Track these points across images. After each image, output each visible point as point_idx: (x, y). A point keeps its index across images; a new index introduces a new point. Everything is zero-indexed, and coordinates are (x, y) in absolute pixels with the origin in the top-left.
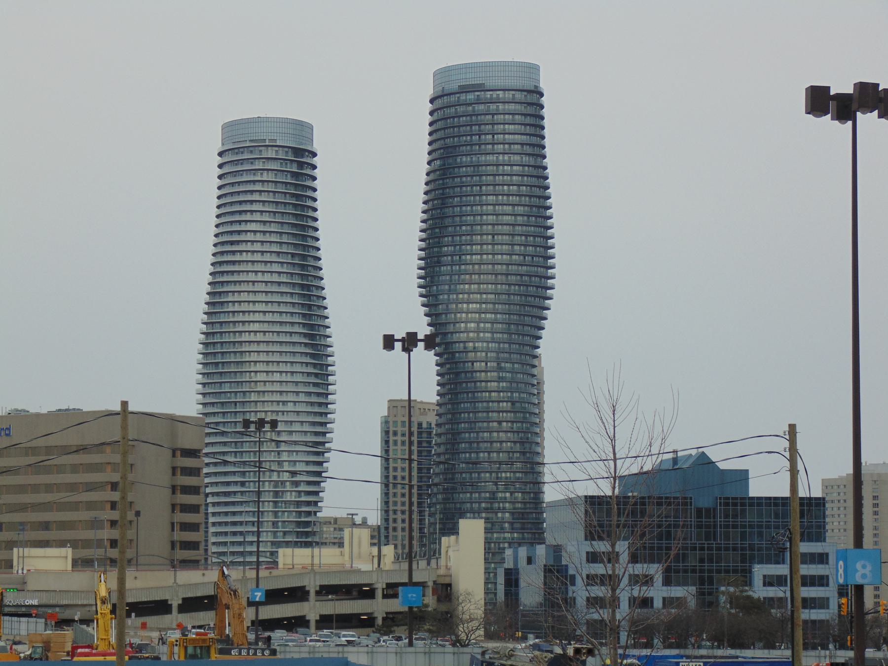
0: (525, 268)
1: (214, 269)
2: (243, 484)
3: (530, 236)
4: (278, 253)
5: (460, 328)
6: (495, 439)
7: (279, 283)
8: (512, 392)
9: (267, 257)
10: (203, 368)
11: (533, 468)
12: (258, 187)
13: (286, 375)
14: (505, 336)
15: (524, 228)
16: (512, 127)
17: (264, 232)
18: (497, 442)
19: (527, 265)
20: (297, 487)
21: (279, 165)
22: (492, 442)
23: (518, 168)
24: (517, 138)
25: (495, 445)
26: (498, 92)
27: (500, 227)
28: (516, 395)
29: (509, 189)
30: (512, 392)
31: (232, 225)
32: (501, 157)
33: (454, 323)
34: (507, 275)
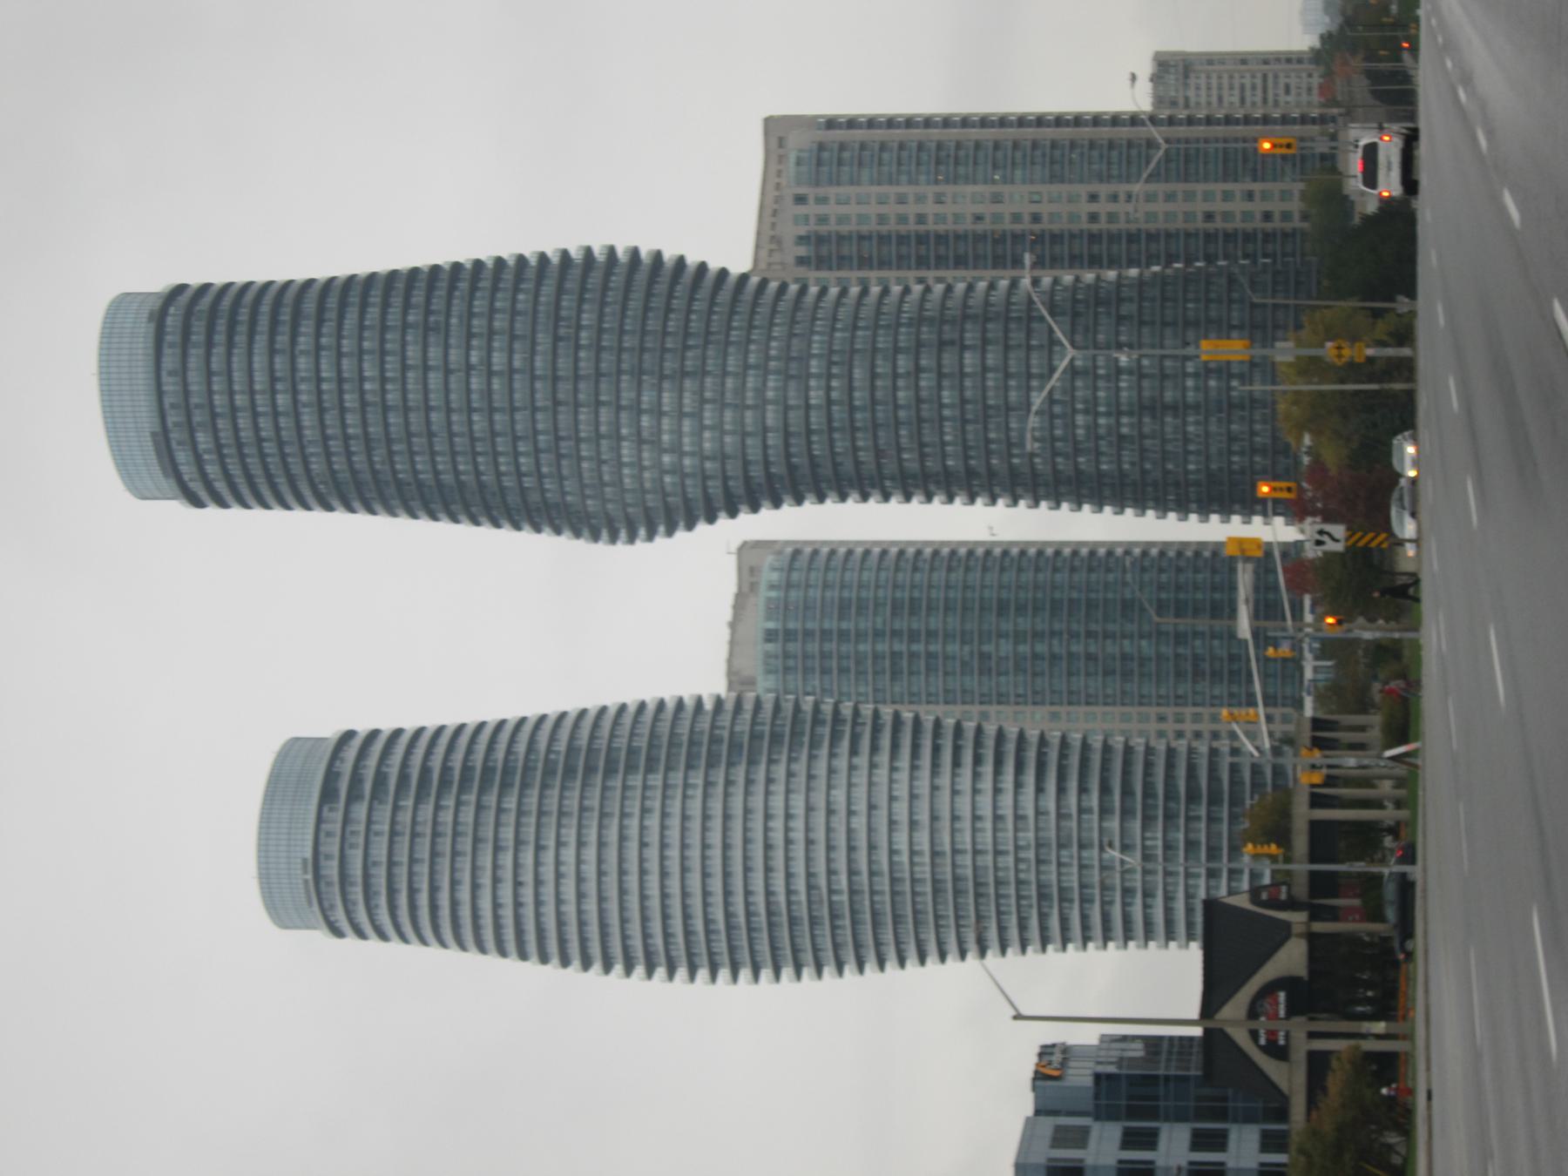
0: (540, 337)
1: (808, 965)
2: (1148, 894)
3: (469, 326)
4: (539, 848)
5: (674, 484)
6: (913, 413)
7: (581, 844)
8: (809, 376)
9: (548, 872)
10: (722, 965)
11: (931, 321)
12: (486, 904)
13: (649, 798)
14: (688, 383)
15: (452, 341)
16: (237, 375)
17: (496, 880)
18: (918, 410)
19: (534, 332)
20: (741, 746)
21: (329, 863)
22: (920, 420)
23: (366, 365)
24: (259, 361)
25: (925, 414)
26: (167, 406)
27: (453, 397)
28: (815, 366)
29: (545, 432)
30: (809, 376)
31: (778, 949)
32: (303, 398)
33: (665, 494)
34: (555, 379)
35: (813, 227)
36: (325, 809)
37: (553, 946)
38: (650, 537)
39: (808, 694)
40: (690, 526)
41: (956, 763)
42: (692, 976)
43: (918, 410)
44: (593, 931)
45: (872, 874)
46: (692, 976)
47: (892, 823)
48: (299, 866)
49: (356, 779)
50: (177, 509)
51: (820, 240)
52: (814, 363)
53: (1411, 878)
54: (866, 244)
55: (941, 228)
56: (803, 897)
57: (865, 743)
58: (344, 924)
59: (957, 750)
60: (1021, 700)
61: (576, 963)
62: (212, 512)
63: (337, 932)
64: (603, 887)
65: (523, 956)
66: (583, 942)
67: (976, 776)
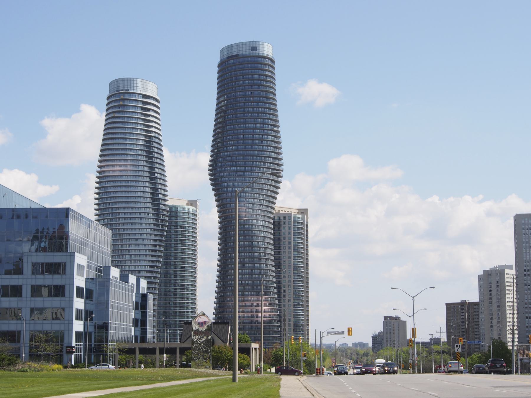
18: (266, 146)
35: (283, 221)
36: (141, 96)
37: (104, 153)
38: (210, 175)
39: (160, 276)
40: (213, 190)
41: (152, 256)
42: (97, 183)
43: (266, 146)
44: (110, 147)
45: (124, 229)
46: (97, 183)
47: (137, 239)
48: (127, 89)
49: (149, 110)
50: (218, 60)
51: (279, 223)
52: (243, 254)
53: (151, 195)
54: (278, 234)
55: (282, 253)
56: (118, 211)
57: (153, 253)
58: (110, 100)
59: (155, 256)
60: (159, 326)
61: (99, 164)
62: (217, 69)
63: (108, 98)
64: (120, 155)
65: (102, 145)
66: (108, 144)
67: (149, 261)
